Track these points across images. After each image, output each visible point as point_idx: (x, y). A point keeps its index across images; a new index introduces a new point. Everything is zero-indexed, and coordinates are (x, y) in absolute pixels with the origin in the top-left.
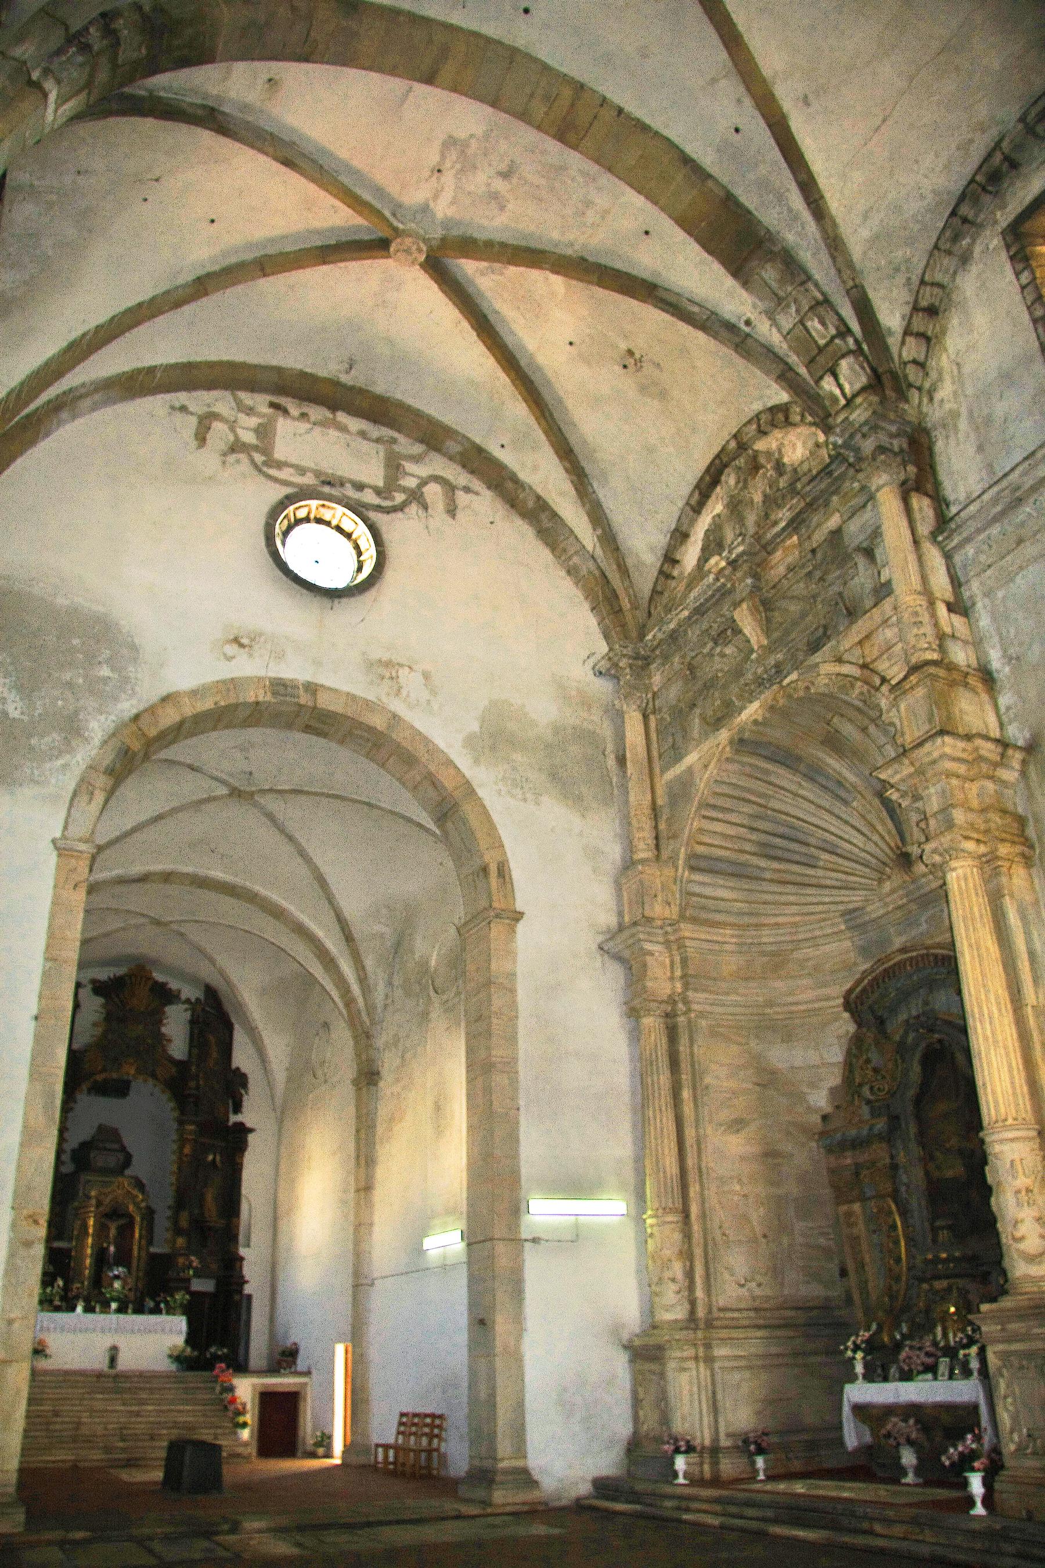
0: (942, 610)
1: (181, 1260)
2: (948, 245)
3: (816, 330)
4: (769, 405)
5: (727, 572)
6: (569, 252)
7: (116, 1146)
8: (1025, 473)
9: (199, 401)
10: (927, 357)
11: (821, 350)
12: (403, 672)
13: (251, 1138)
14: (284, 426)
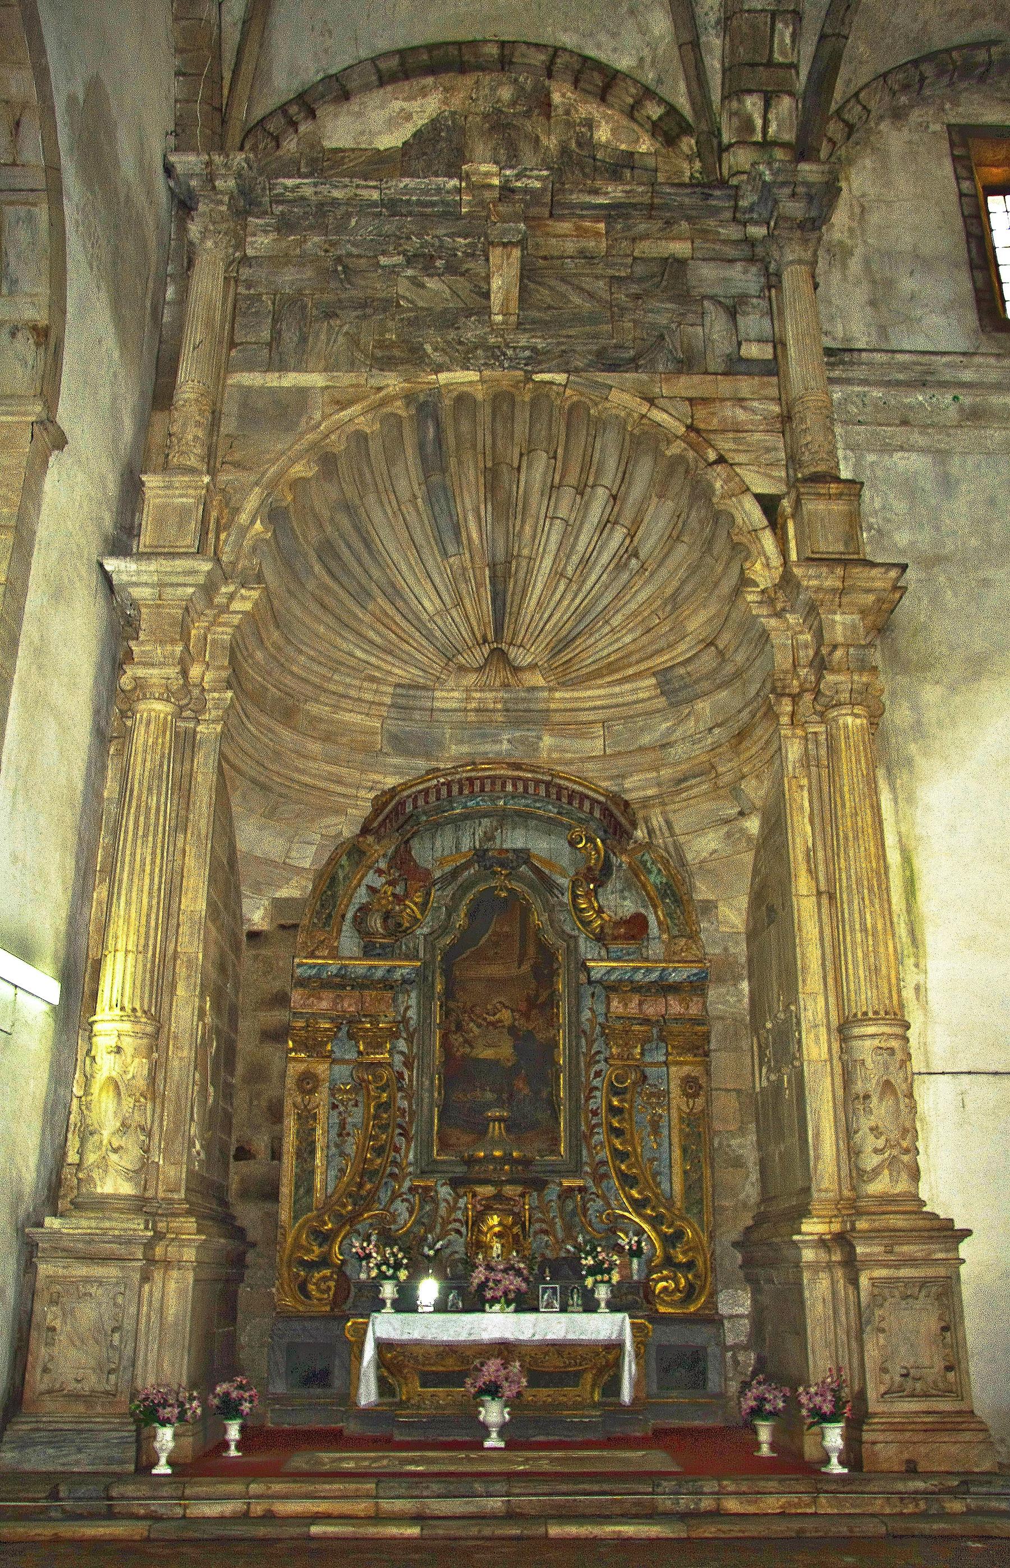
2: (896, 87)
3: (782, 41)
4: (592, 52)
5: (488, 195)
11: (770, 64)
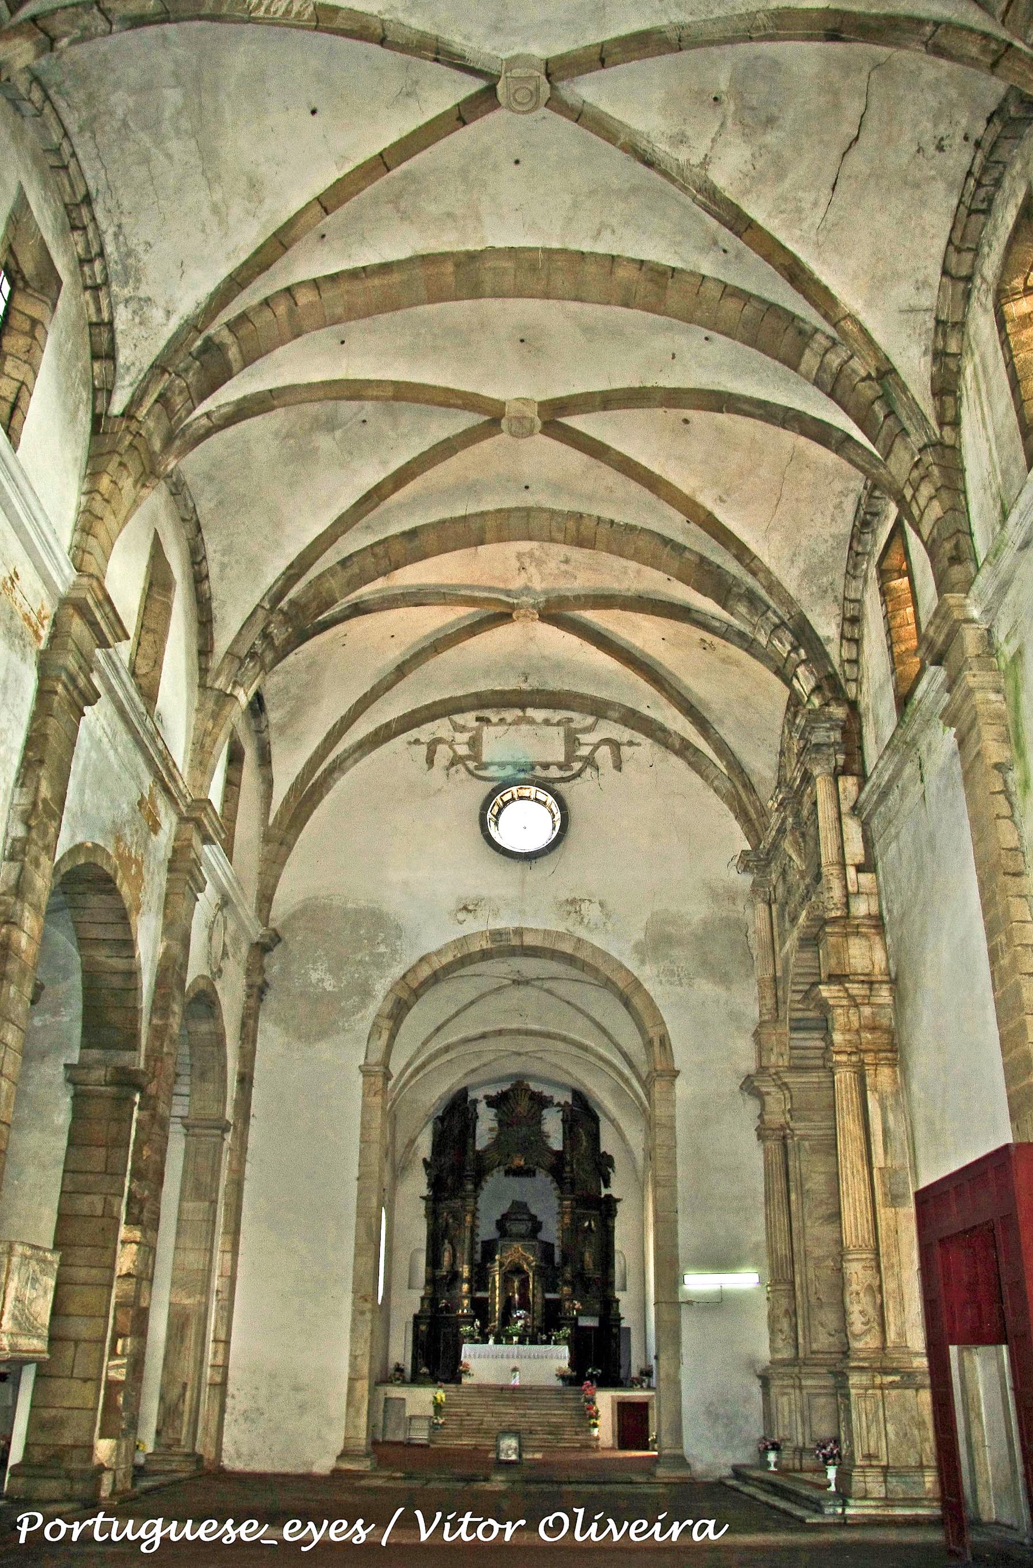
0: (851, 872)
1: (567, 1304)
6: (630, 594)
7: (525, 1217)
8: (878, 777)
9: (425, 732)
10: (858, 655)
12: (585, 906)
13: (619, 1207)
14: (488, 733)
